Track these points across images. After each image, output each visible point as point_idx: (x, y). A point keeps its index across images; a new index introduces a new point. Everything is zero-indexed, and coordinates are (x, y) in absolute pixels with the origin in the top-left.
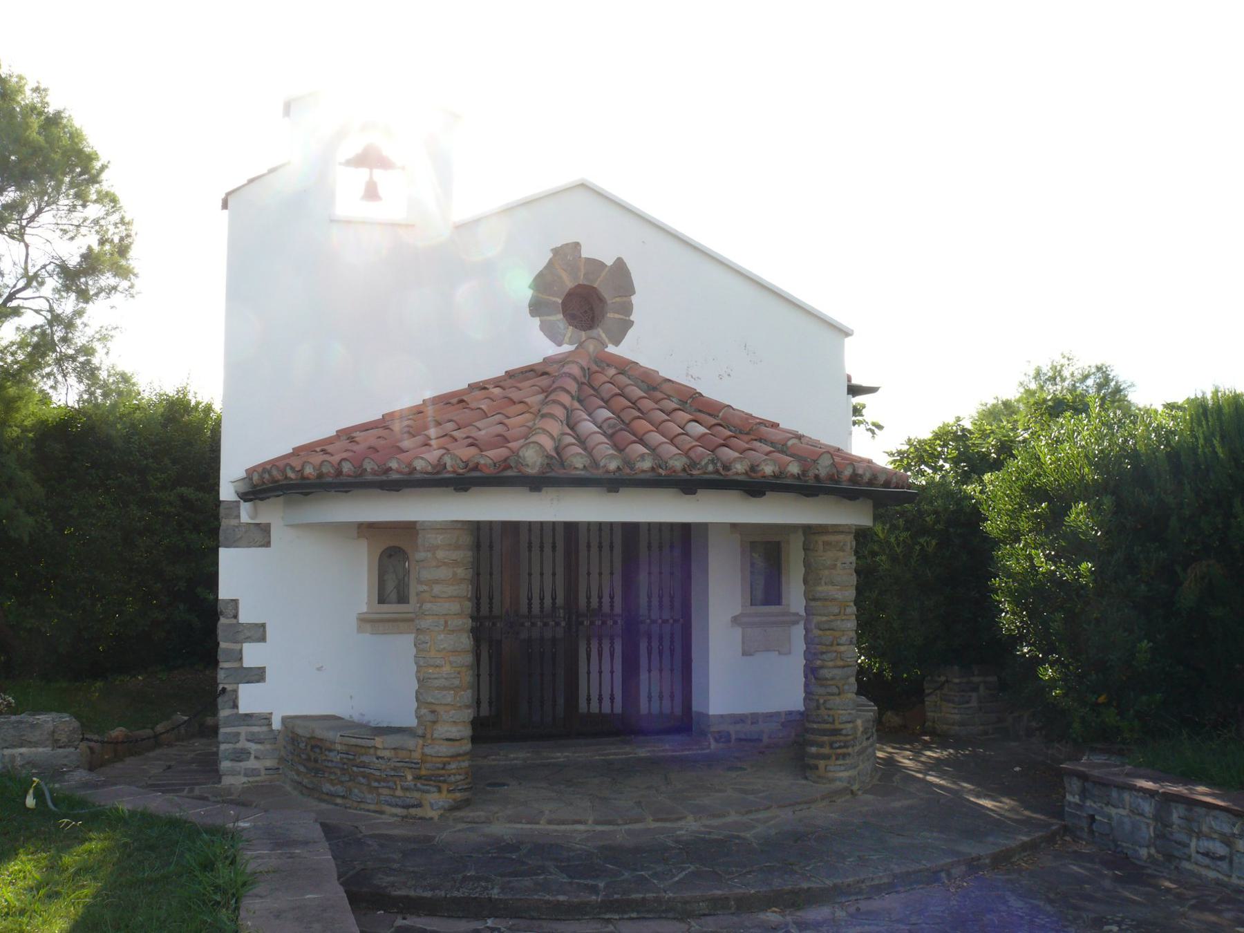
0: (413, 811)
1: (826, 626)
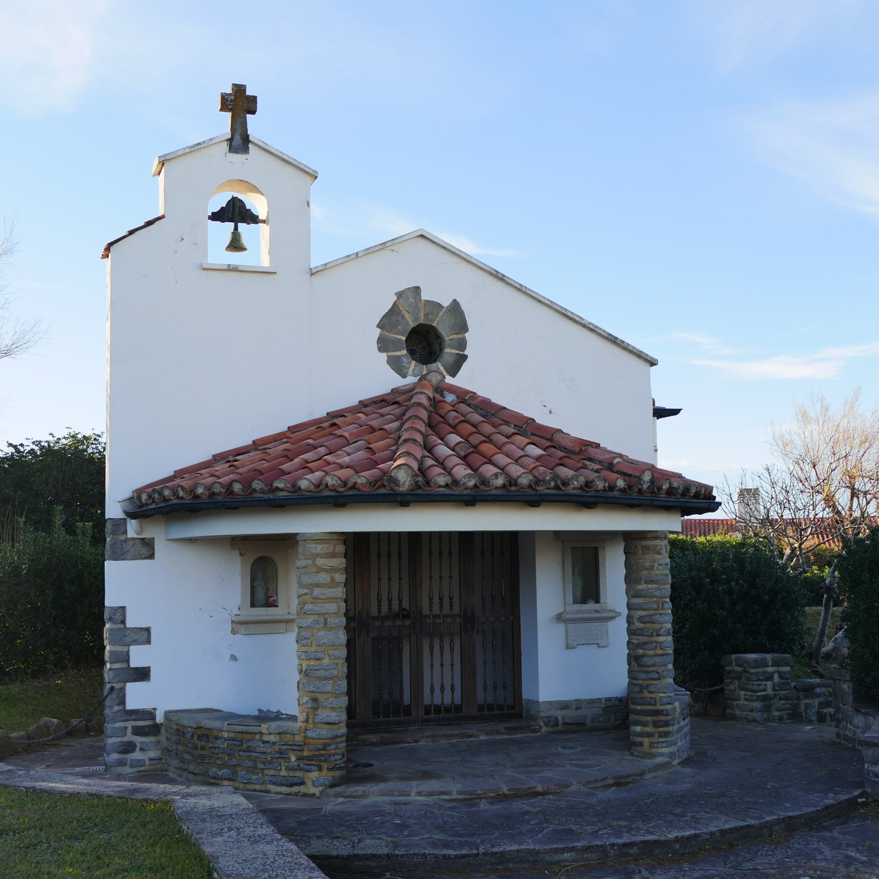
0: (295, 789)
1: (647, 619)
